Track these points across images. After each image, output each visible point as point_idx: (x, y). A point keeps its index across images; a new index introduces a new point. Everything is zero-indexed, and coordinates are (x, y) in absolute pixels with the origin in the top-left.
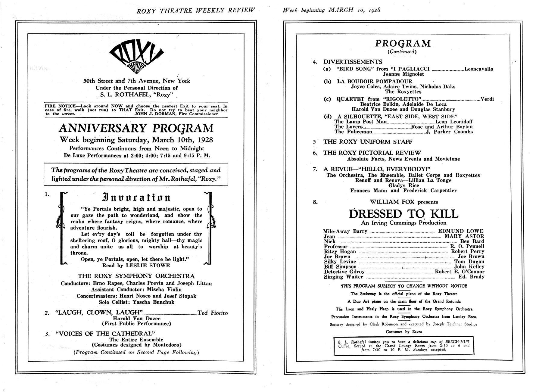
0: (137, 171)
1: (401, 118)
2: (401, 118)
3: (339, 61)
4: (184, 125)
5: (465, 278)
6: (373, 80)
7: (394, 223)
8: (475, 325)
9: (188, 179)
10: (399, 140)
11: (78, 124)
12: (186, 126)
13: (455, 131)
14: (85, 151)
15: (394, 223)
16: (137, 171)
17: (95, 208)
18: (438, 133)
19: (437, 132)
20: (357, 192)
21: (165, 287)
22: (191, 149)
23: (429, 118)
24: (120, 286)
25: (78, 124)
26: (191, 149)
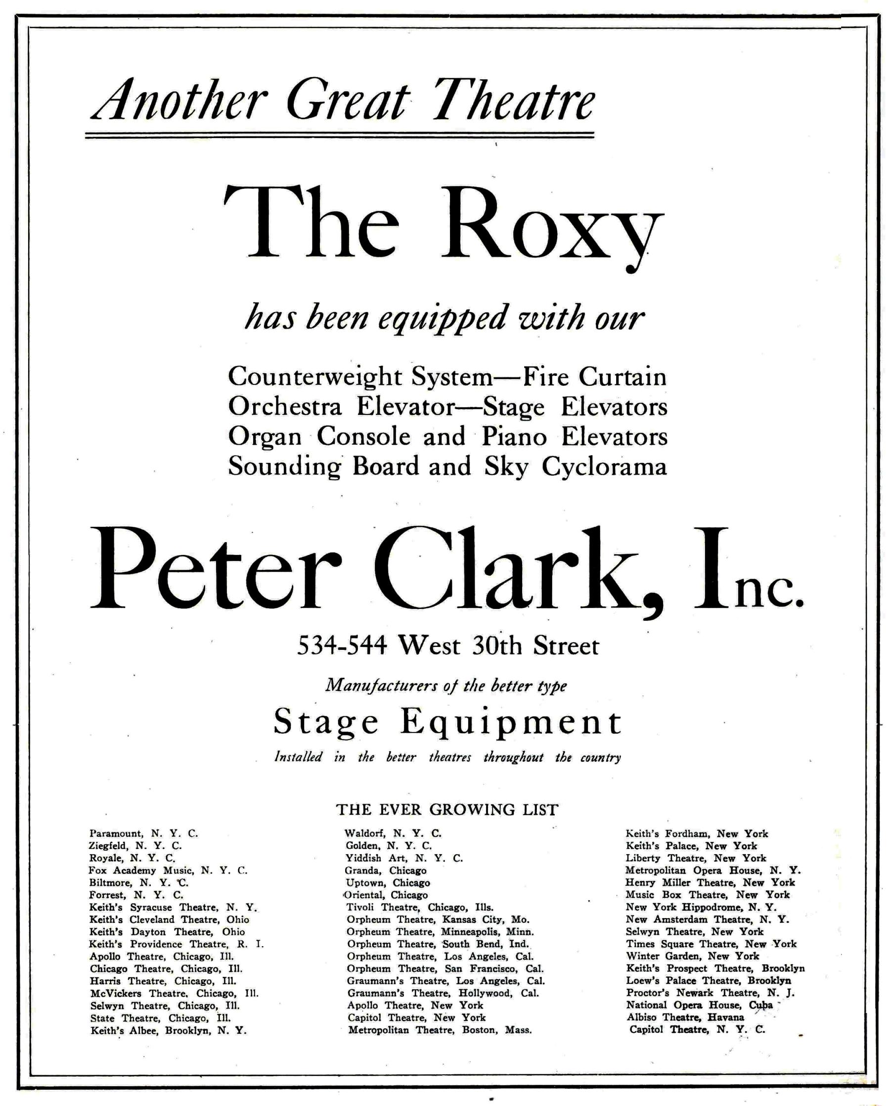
0: (416, 933)
1: (552, 814)
2: (552, 814)
3: (411, 807)
4: (440, 805)
5: (525, 946)
6: (418, 807)
7: (601, 375)
8: (650, 1006)
9: (371, 687)
10: (552, 806)
11: (750, 606)
12: (442, 807)
13: (189, 832)
14: (489, 948)
15: (601, 375)
16: (416, 933)
17: (93, 832)
18: (97, 836)
19: (96, 834)
20: (358, 873)
21: (690, 876)
22: (717, 908)
23: (404, 813)
24: (699, 863)
25: (750, 606)
26: (717, 908)
